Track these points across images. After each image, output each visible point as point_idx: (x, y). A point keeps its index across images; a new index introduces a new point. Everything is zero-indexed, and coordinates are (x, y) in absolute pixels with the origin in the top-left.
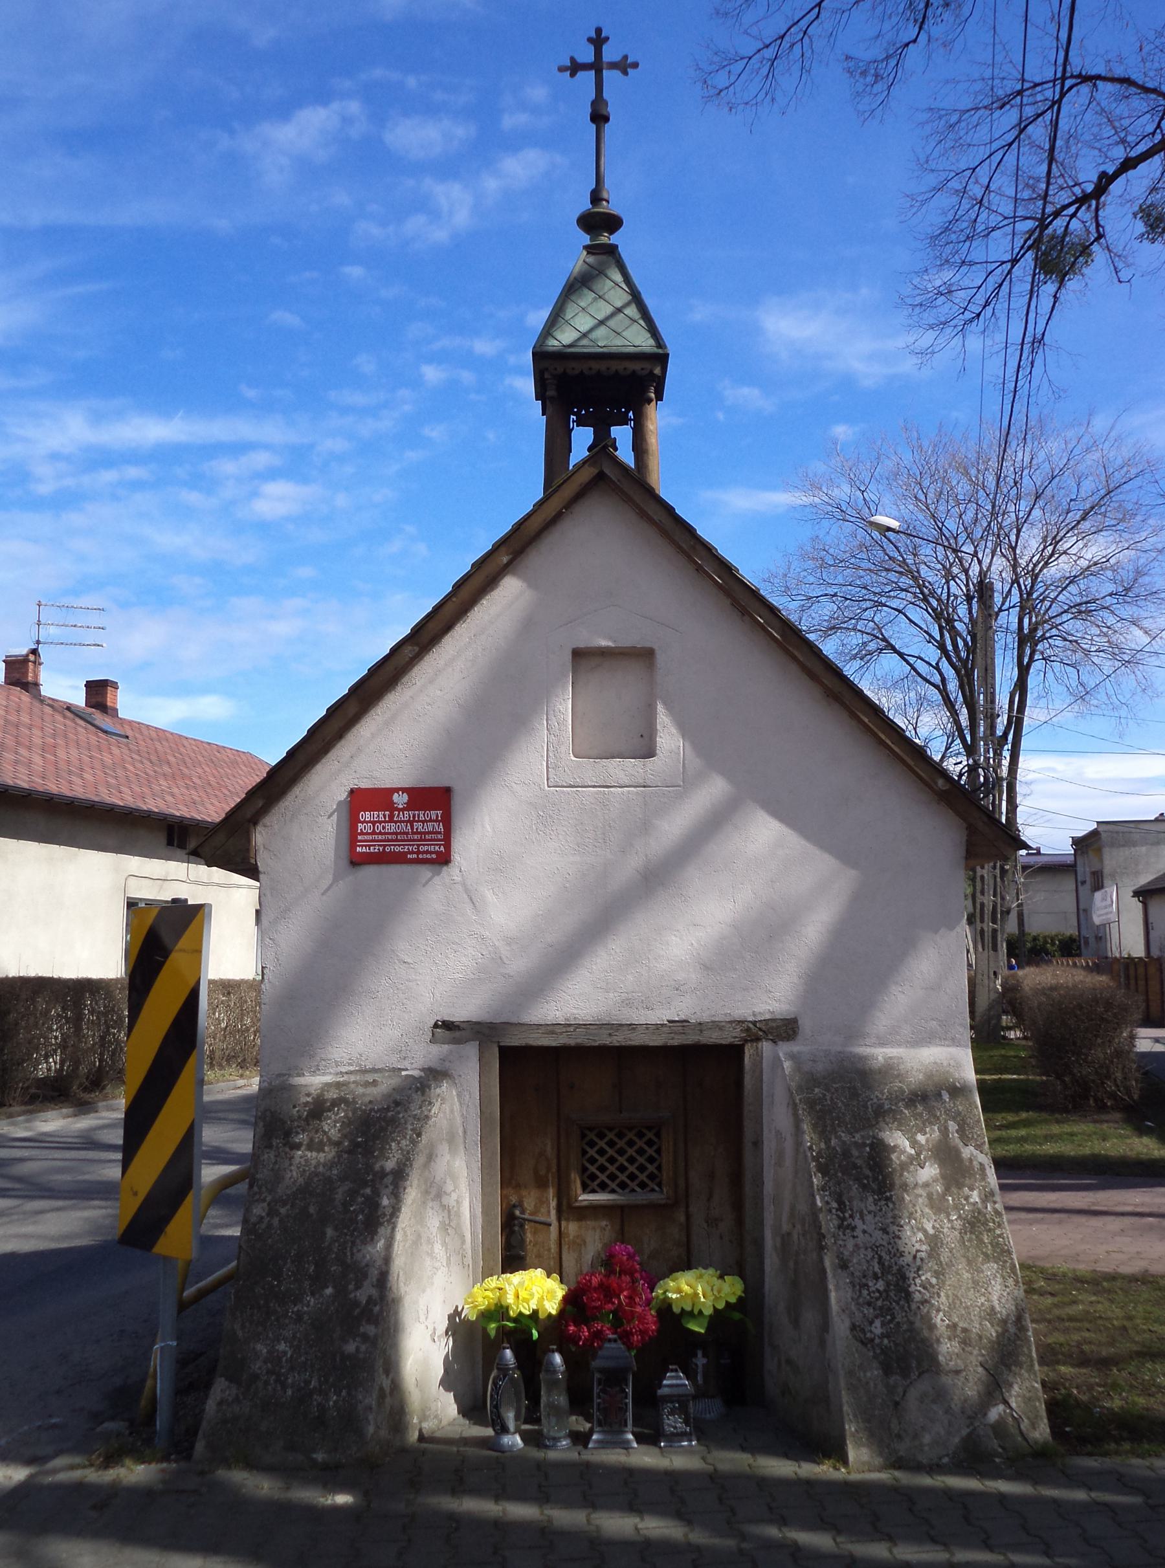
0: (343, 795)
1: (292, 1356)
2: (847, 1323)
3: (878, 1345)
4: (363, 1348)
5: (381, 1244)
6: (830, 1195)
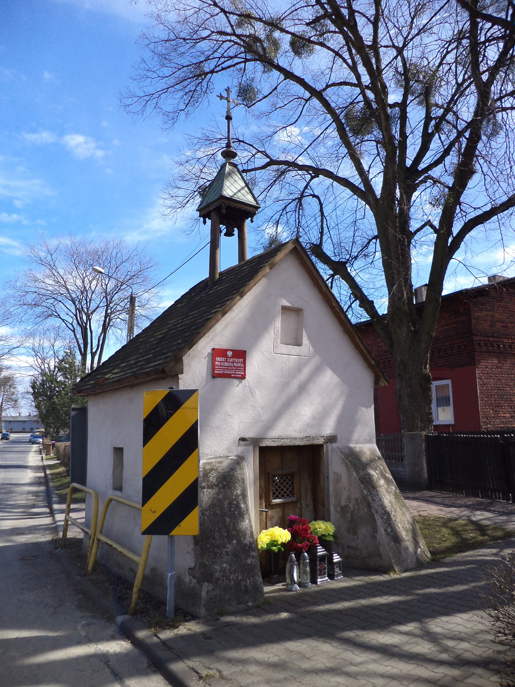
0: (209, 351)
4: (253, 561)
5: (247, 521)
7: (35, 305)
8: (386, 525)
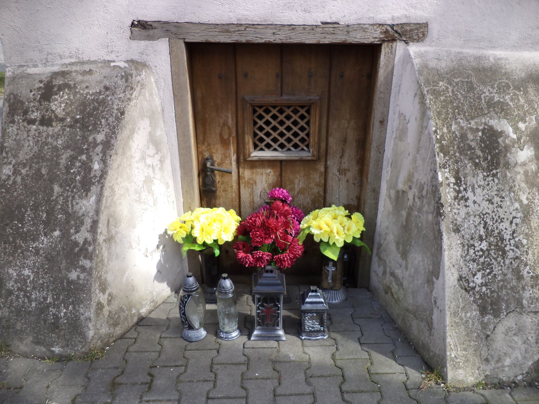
1: (33, 279)
2: (456, 276)
3: (477, 292)
4: (82, 276)
5: (93, 199)
6: (449, 172)
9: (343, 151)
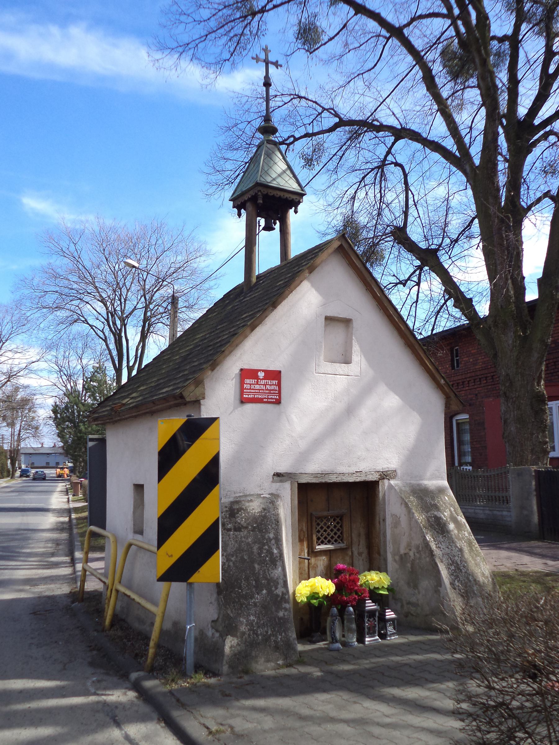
7: (56, 308)
8: (453, 577)
9: (359, 542)
